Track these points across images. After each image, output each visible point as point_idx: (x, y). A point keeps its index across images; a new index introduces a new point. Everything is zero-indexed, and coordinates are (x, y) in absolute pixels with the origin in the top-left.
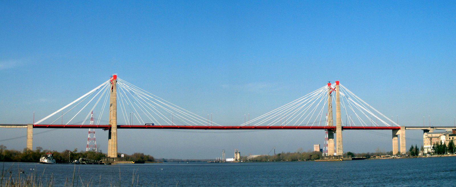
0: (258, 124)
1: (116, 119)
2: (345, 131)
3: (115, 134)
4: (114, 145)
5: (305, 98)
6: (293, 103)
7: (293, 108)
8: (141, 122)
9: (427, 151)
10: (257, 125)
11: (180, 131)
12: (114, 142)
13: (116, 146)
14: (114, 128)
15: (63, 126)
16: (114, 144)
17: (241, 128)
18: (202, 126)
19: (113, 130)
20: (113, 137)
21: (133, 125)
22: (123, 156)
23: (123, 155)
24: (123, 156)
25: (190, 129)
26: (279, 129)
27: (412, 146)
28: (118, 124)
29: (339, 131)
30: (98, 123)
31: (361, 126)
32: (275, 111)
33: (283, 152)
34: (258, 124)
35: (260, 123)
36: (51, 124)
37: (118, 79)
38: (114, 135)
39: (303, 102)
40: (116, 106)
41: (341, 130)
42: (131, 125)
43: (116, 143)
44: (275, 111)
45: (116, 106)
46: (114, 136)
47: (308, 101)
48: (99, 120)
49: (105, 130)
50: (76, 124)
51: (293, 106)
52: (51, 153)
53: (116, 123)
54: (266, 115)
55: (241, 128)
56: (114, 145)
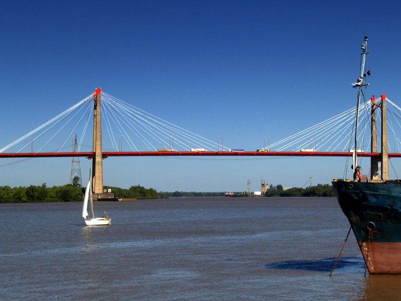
2: (392, 159)
6: (329, 121)
7: (305, 131)
8: (134, 149)
11: (226, 159)
16: (99, 176)
17: (258, 154)
19: (98, 159)
23: (110, 190)
27: (45, 183)
29: (385, 159)
33: (319, 185)
39: (341, 120)
41: (387, 158)
42: (121, 151)
43: (100, 175)
47: (347, 119)
49: (89, 158)
51: (332, 123)
52: (111, 188)
53: (101, 150)
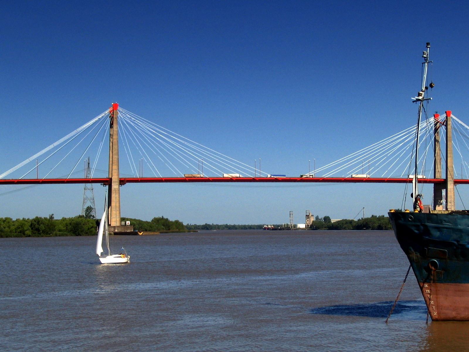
0: (327, 175)
1: (118, 169)
2: (459, 186)
3: (117, 191)
4: (116, 207)
5: (405, 133)
9: (118, 214)
10: (326, 176)
12: (116, 203)
13: (118, 209)
14: (115, 182)
15: (363, 180)
17: (302, 180)
18: (217, 177)
19: (115, 186)
20: (114, 195)
21: (143, 177)
22: (128, 223)
23: (129, 222)
24: (128, 223)
25: (328, 182)
26: (246, 182)
28: (121, 177)
30: (91, 177)
31: (154, 177)
32: (355, 154)
34: (327, 175)
35: (330, 174)
36: (21, 177)
37: (119, 108)
38: (116, 192)
40: (118, 150)
42: (141, 177)
44: (355, 154)
45: (117, 149)
46: (116, 194)
48: (94, 169)
49: (104, 185)
50: (396, 178)
54: (342, 160)
55: (302, 180)
56: (115, 207)
